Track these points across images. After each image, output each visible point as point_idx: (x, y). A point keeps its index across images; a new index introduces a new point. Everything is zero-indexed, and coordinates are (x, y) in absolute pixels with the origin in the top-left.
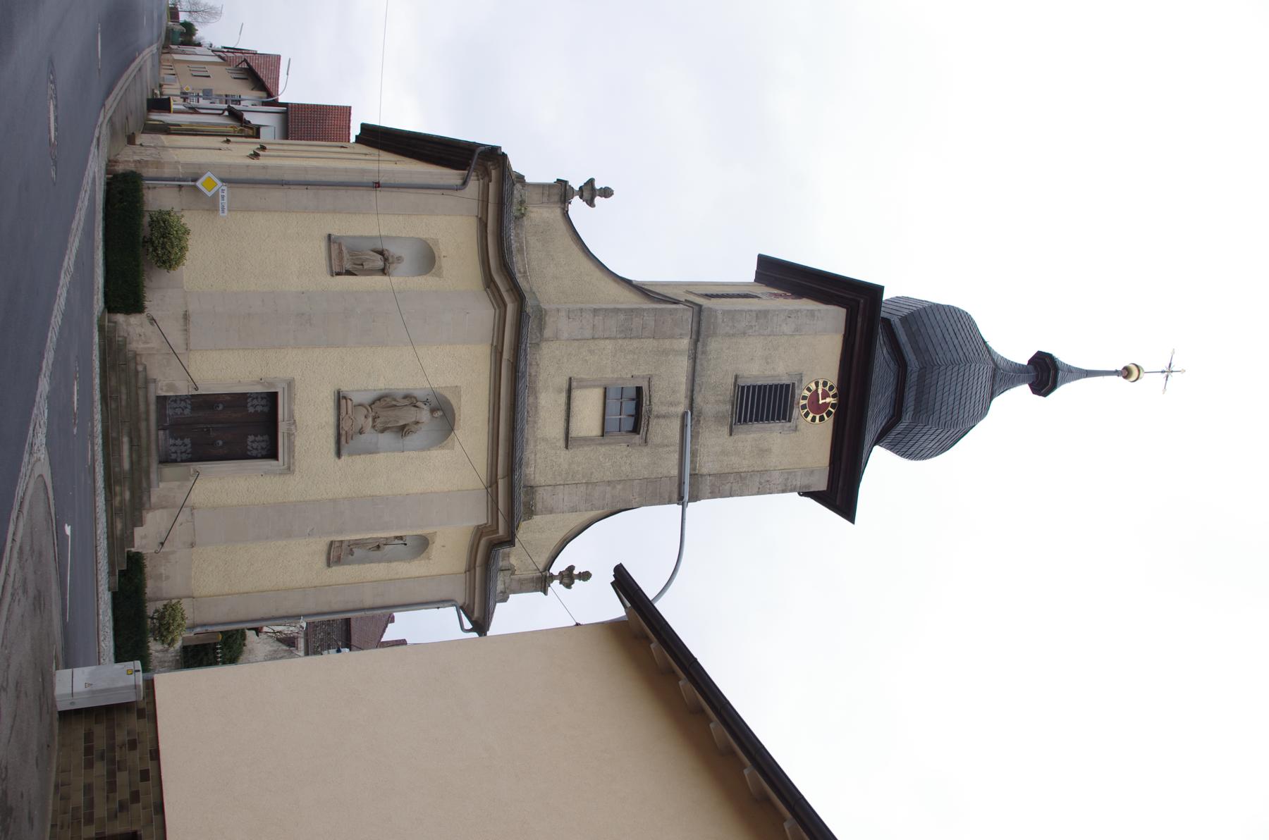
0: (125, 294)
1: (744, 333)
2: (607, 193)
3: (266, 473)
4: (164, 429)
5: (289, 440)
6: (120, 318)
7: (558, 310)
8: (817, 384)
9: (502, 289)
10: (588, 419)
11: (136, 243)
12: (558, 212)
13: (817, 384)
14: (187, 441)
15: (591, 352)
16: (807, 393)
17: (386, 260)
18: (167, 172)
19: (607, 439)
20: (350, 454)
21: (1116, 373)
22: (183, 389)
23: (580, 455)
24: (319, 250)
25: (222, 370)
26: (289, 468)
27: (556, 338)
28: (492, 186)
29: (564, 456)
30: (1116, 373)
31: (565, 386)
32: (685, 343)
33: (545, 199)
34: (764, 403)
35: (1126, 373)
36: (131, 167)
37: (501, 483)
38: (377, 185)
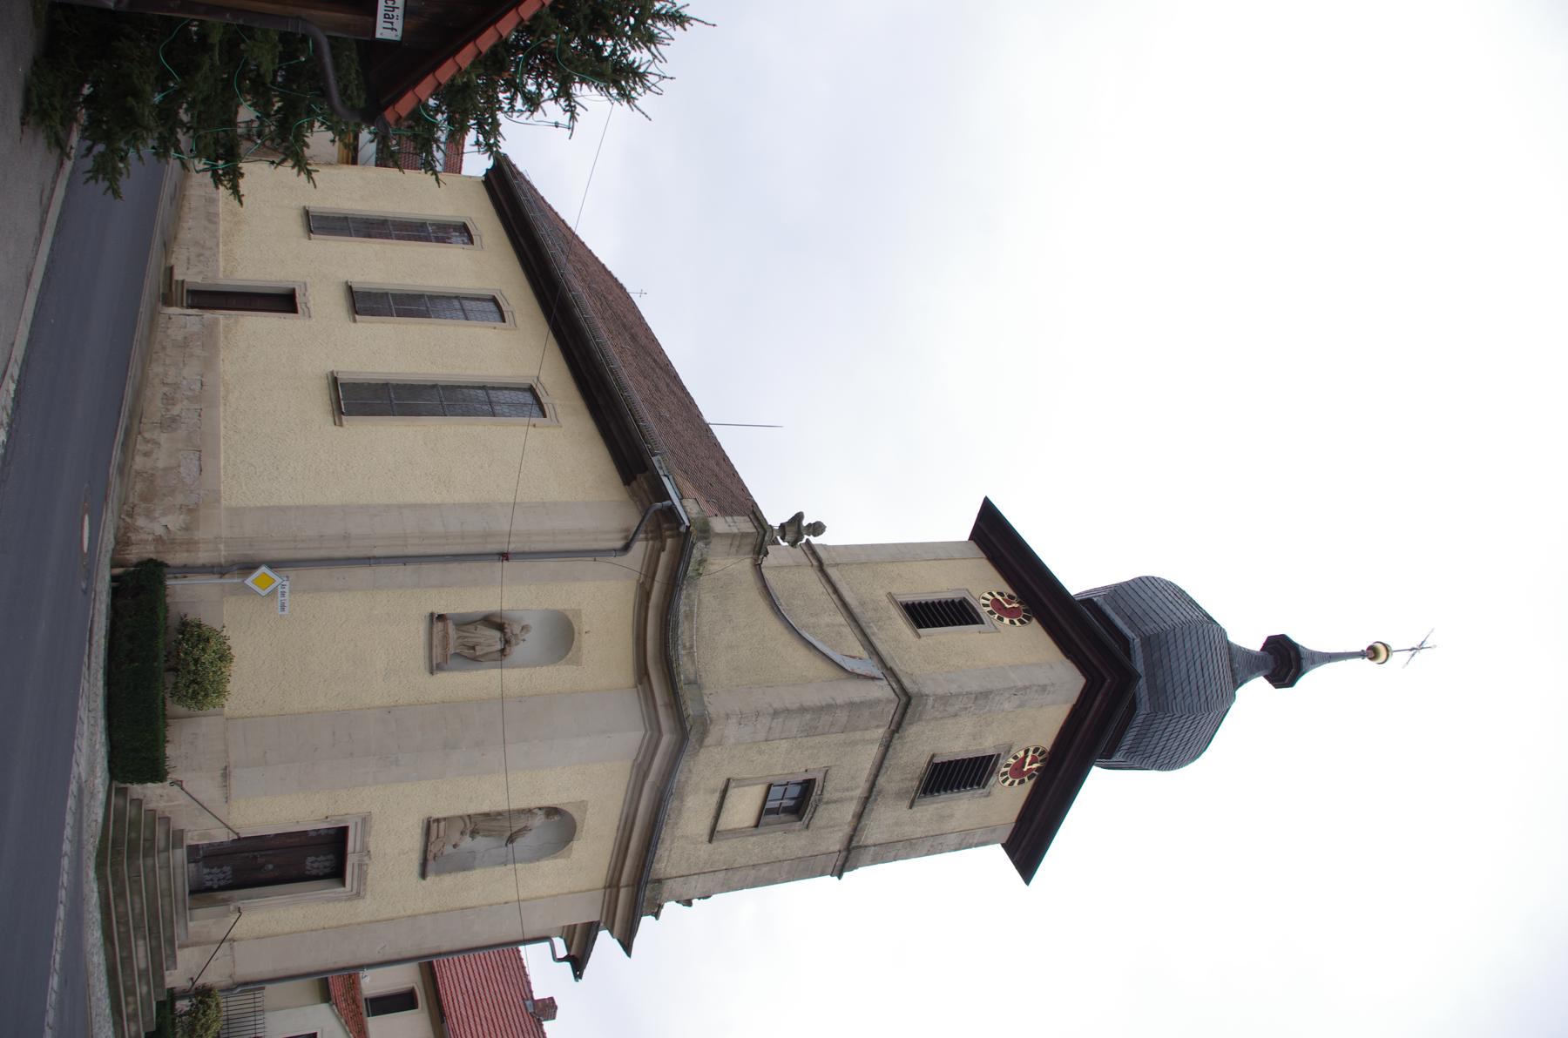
0: (137, 753)
1: (955, 715)
3: (328, 901)
4: (195, 862)
5: (360, 881)
6: (136, 790)
7: (728, 716)
8: (1027, 752)
9: (659, 702)
10: (743, 807)
11: (155, 662)
12: (746, 563)
13: (1027, 752)
14: (227, 869)
15: (760, 752)
16: (1012, 761)
17: (507, 642)
18: (203, 557)
19: (760, 829)
20: (439, 873)
21: (1362, 655)
22: (221, 836)
23: (723, 847)
24: (415, 635)
25: (272, 809)
26: (358, 894)
27: (720, 743)
28: (664, 558)
29: (705, 849)
30: (1362, 655)
31: (721, 786)
32: (880, 733)
33: (734, 550)
34: (956, 776)
35: (1372, 653)
36: (148, 552)
37: (623, 893)
38: (505, 556)
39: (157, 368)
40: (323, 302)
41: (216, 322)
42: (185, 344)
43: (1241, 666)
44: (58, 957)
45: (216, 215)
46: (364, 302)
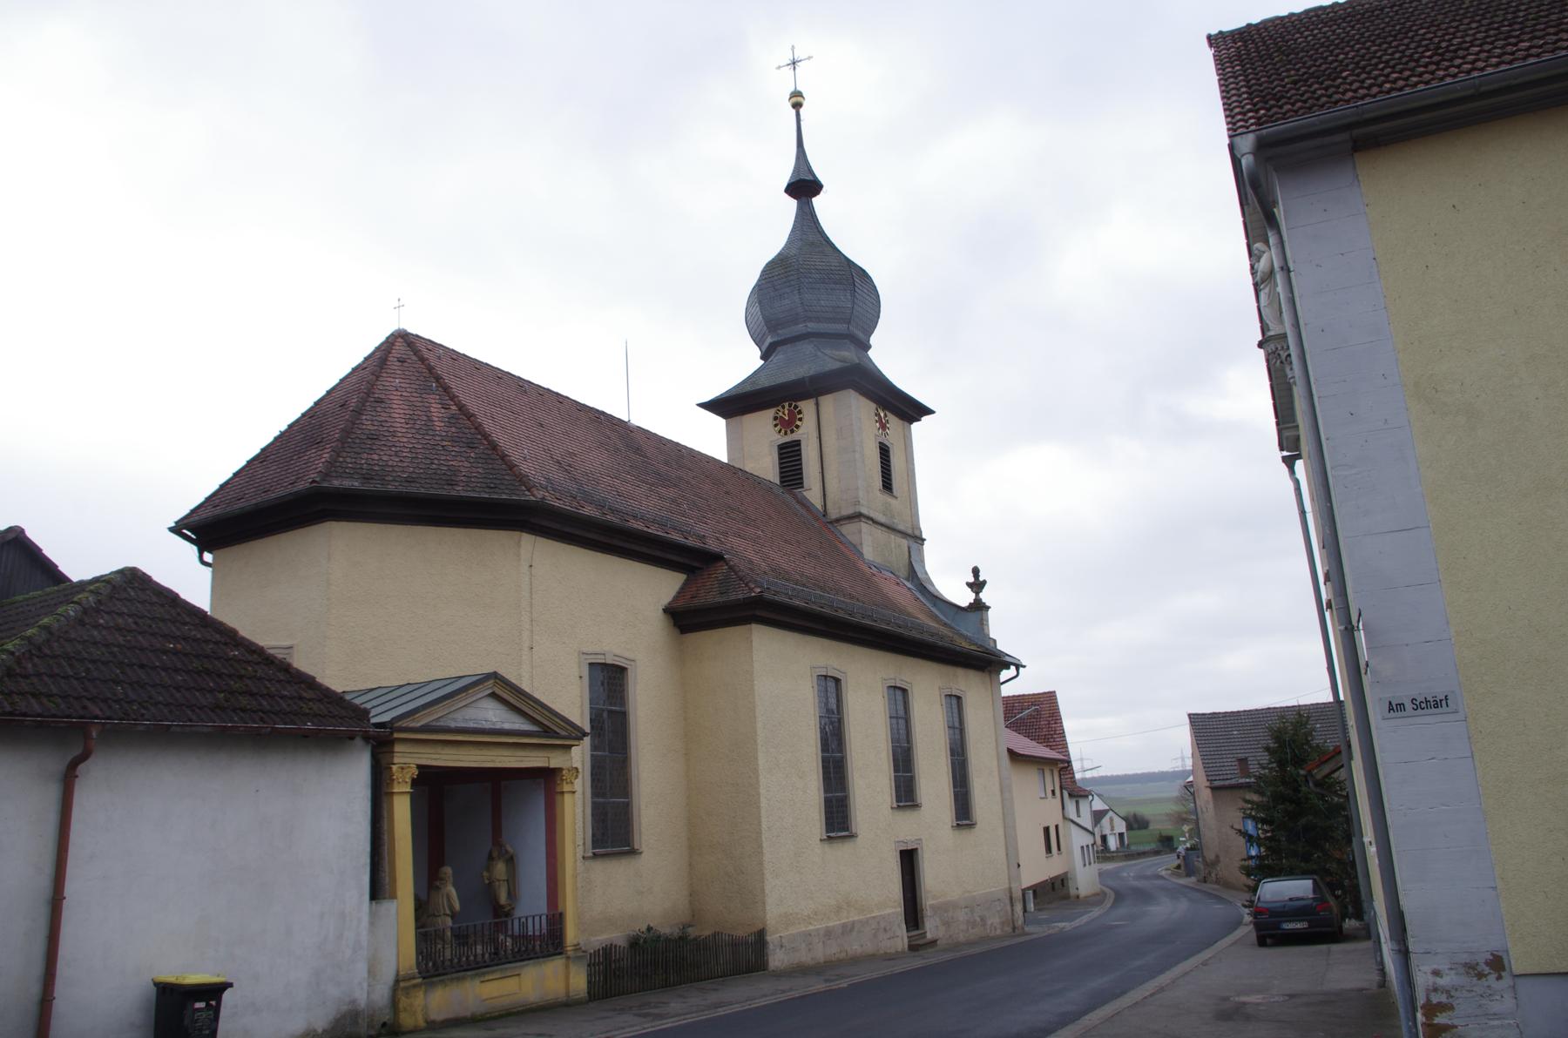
2: (976, 571)
35: (797, 106)
39: (962, 938)
40: (907, 828)
41: (932, 906)
42: (947, 924)
43: (807, 222)
44: (1085, 919)
45: (844, 926)
46: (906, 794)
